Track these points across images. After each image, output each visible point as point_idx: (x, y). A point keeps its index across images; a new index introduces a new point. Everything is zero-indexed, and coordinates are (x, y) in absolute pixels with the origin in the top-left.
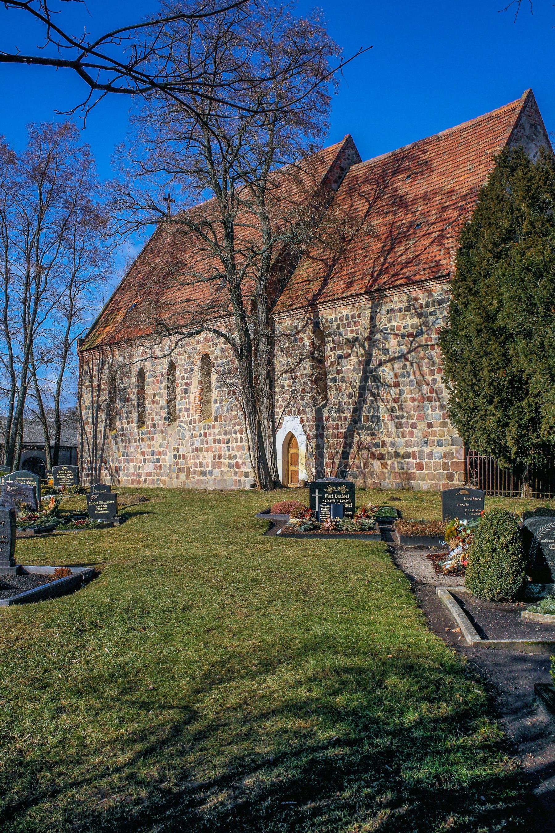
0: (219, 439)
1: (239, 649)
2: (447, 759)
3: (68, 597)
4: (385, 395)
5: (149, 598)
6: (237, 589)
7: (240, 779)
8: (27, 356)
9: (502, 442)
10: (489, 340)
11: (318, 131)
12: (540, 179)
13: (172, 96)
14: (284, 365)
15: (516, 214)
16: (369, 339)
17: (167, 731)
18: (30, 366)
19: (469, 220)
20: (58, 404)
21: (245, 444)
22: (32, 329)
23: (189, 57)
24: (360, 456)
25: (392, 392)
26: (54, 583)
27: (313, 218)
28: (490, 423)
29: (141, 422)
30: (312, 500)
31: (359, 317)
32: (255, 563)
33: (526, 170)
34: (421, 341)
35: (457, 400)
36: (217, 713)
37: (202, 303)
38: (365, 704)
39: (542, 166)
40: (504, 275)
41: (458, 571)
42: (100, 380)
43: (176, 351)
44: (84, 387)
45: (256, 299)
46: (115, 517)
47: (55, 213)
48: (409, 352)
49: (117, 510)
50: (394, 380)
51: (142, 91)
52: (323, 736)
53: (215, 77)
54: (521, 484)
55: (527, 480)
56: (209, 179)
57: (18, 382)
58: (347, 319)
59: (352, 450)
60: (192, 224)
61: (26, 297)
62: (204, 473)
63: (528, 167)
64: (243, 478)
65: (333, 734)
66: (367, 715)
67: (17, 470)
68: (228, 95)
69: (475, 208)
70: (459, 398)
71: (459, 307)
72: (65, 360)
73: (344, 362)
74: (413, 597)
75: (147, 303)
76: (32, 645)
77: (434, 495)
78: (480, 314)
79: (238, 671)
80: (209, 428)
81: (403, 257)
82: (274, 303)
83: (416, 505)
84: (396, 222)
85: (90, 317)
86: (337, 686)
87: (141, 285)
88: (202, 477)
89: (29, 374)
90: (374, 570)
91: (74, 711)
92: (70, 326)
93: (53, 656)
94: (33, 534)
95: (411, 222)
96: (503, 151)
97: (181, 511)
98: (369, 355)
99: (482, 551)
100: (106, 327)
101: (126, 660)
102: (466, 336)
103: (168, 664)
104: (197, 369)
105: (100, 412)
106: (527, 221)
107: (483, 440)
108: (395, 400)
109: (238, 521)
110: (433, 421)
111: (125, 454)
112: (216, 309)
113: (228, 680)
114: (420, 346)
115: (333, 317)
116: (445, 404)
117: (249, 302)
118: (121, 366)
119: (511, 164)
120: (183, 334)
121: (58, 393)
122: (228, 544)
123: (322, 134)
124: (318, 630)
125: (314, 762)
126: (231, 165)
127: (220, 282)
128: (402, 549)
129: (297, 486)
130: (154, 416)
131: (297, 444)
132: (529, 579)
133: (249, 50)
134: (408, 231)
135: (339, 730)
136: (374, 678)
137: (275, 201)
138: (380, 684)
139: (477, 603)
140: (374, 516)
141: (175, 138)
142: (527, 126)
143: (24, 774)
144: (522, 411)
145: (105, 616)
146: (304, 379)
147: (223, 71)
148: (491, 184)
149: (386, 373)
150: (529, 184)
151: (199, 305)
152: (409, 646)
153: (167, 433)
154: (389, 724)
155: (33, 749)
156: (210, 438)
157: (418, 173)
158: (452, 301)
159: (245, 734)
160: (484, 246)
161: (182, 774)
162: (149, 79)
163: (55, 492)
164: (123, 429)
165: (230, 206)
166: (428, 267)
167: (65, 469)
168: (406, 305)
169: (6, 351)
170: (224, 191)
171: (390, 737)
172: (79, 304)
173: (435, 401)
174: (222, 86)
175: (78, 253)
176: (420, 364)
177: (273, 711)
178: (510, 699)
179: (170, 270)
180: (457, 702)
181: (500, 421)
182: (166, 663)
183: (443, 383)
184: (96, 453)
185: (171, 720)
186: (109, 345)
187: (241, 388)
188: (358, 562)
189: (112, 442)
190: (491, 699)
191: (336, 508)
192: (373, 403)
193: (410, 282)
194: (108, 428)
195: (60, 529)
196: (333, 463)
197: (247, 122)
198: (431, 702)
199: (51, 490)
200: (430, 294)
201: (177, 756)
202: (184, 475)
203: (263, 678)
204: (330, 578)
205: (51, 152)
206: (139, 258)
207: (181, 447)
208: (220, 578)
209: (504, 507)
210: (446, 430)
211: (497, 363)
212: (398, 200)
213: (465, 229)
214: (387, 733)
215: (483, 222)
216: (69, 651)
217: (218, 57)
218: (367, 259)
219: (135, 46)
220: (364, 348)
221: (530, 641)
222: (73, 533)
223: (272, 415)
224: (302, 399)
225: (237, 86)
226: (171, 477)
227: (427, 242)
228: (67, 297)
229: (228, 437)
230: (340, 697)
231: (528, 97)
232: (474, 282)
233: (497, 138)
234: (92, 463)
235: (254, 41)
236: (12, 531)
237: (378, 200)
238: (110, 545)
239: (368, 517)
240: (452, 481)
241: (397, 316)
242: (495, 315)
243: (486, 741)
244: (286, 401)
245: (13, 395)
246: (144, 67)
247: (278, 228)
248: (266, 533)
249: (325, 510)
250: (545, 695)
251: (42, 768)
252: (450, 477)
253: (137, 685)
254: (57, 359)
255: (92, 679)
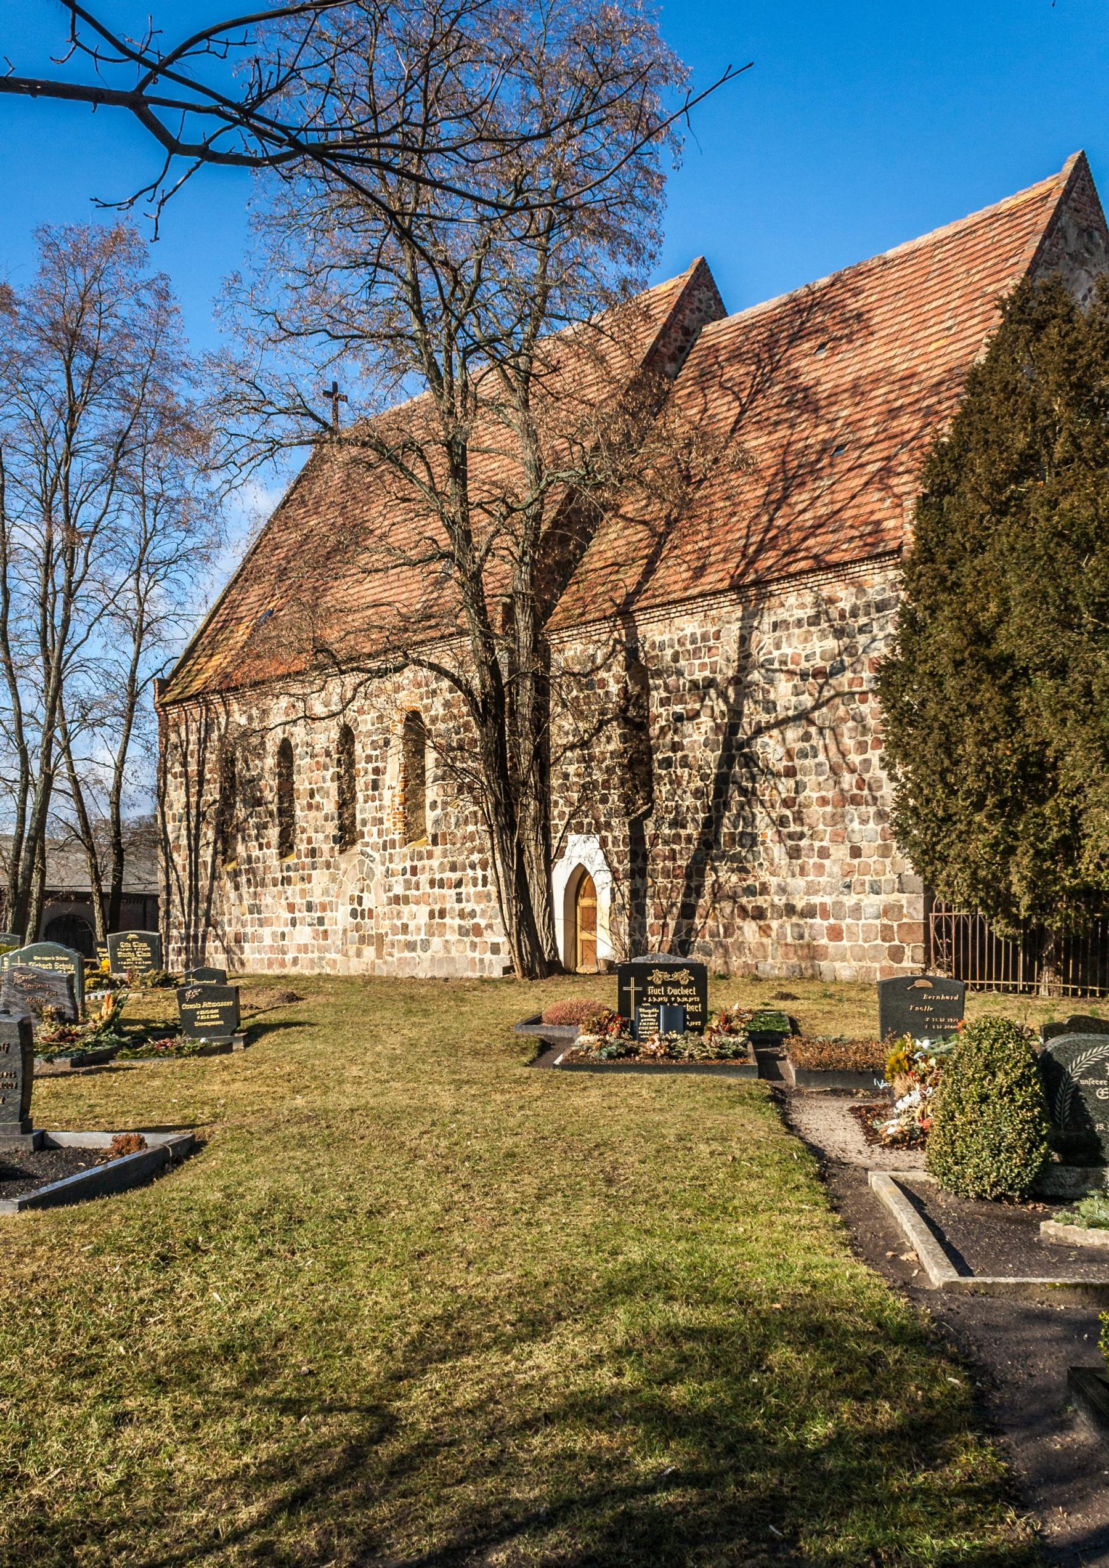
0: (442, 880)
1: (479, 1292)
2: (893, 1516)
3: (138, 1192)
4: (767, 793)
5: (303, 1192)
6: (475, 1173)
7: (480, 1553)
8: (52, 711)
9: (1002, 886)
10: (980, 680)
11: (638, 249)
12: (1094, 347)
13: (338, 172)
14: (567, 733)
15: (1042, 421)
16: (736, 681)
17: (336, 1457)
18: (58, 733)
19: (943, 435)
20: (118, 809)
21: (492, 888)
22: (60, 658)
23: (370, 87)
24: (717, 912)
25: (780, 787)
26: (110, 1165)
27: (627, 436)
28: (978, 848)
29: (286, 846)
30: (623, 997)
31: (718, 638)
32: (512, 1122)
33: (1066, 328)
34: (841, 684)
35: (911, 802)
36: (435, 1420)
37: (404, 610)
38: (728, 1401)
39: (1100, 318)
40: (1013, 549)
41: (911, 1139)
42: (202, 763)
43: (355, 705)
44: (169, 776)
45: (513, 603)
46: (234, 1032)
47: (100, 421)
48: (817, 706)
49: (233, 1018)
50: (785, 763)
51: (275, 160)
52: (646, 1465)
53: (425, 133)
54: (1040, 968)
55: (1051, 961)
56: (417, 353)
57: (35, 766)
58: (693, 642)
59: (701, 902)
60: (383, 446)
61: (46, 592)
62: (411, 946)
63: (1070, 321)
64: (488, 956)
65: (664, 1461)
66: (733, 1423)
67: (34, 941)
68: (453, 171)
69: (958, 410)
70: (916, 798)
71: (920, 615)
72: (130, 722)
73: (688, 727)
74: (822, 1190)
75: (295, 608)
76: (65, 1290)
77: (864, 990)
78: (960, 629)
79: (478, 1335)
80: (421, 859)
81: (808, 515)
82: (548, 610)
83: (827, 1008)
84: (794, 442)
85: (179, 636)
86: (672, 1364)
87: (283, 573)
88: (407, 954)
89: (56, 750)
90: (744, 1137)
91: (150, 1421)
92: (138, 653)
93: (108, 1313)
94: (68, 1069)
95: (824, 441)
96: (1019, 289)
97: (367, 1019)
98: (736, 713)
99: (960, 1101)
100: (212, 655)
101: (256, 1317)
102: (931, 673)
103: (339, 1323)
104: (396, 743)
105: (203, 826)
106: (1064, 434)
107: (962, 881)
108: (787, 803)
109: (478, 1038)
110: (864, 845)
111: (254, 909)
112: (433, 622)
113: (458, 1353)
114: (838, 694)
115: (666, 637)
116: (888, 809)
117: (500, 609)
118: (245, 734)
119: (1034, 315)
120: (369, 671)
121: (118, 788)
122: (459, 1084)
123: (646, 256)
124: (636, 1254)
125: (628, 1517)
126: (461, 324)
127: (439, 566)
128: (799, 1094)
129: (594, 970)
130: (313, 835)
131: (593, 888)
132: (1056, 1157)
133: (496, 71)
134: (818, 461)
135: (677, 1453)
136: (746, 1350)
137: (550, 399)
138: (757, 1363)
139: (951, 1204)
140: (745, 1030)
141: (344, 264)
142: (1072, 233)
143: (46, 1549)
144: (1044, 824)
145: (213, 1229)
146: (607, 762)
147: (443, 119)
148: (992, 358)
149: (771, 749)
150: (1072, 357)
151: (399, 614)
152: (814, 1287)
153: (337, 868)
154: (775, 1443)
155: (67, 1498)
156: (423, 878)
157: (841, 338)
158: (904, 604)
159: (491, 1462)
160: (974, 489)
161: (366, 1543)
162: (288, 135)
163: (112, 985)
164: (249, 860)
165: (459, 410)
166: (857, 534)
167: (134, 940)
168: (811, 612)
169: (8, 702)
170: (446, 378)
171: (778, 1470)
172: (158, 607)
173: (867, 804)
174: (440, 151)
175: (151, 504)
176: (838, 731)
177: (546, 1416)
178: (1018, 1396)
179: (340, 542)
180: (912, 1400)
181: (997, 844)
182: (335, 1320)
183: (883, 768)
184: (197, 907)
185: (344, 1436)
186: (219, 692)
187: (484, 779)
188: (714, 1120)
189: (229, 886)
190: (979, 1397)
191: (670, 1013)
192: (742, 808)
193: (821, 566)
194: (220, 857)
195: (124, 1057)
196: (665, 925)
197: (492, 230)
198: (860, 1399)
199: (105, 981)
200: (861, 590)
201: (356, 1507)
202: (372, 949)
203: (527, 1349)
204: (658, 1151)
205: (87, 288)
206: (276, 516)
207: (365, 895)
208: (442, 1151)
209: (1005, 1014)
210: (888, 861)
211: (994, 728)
212: (800, 396)
213: (934, 455)
214: (773, 1461)
215: (974, 438)
216: (142, 1301)
217: (432, 87)
218: (735, 519)
219: (257, 61)
220: (726, 700)
221: (1058, 1281)
222: (150, 1064)
223: (546, 833)
224: (604, 800)
225: (471, 152)
226: (346, 955)
227: (857, 482)
228: (130, 595)
229: (457, 875)
230: (679, 1387)
231: (1076, 168)
232: (952, 564)
233: (1007, 260)
234: (188, 927)
235: (506, 52)
236: (24, 1063)
237: (760, 396)
238: (225, 1088)
239: (732, 1031)
240: (901, 962)
241: (793, 634)
242: (992, 630)
243: (971, 1480)
244: (572, 804)
245: (25, 791)
246: (278, 108)
247: (557, 457)
248: (531, 1063)
249: (648, 1018)
250: (1090, 1391)
251: (84, 1536)
252: (896, 954)
253: (276, 1367)
254: (114, 719)
255: (186, 1355)
